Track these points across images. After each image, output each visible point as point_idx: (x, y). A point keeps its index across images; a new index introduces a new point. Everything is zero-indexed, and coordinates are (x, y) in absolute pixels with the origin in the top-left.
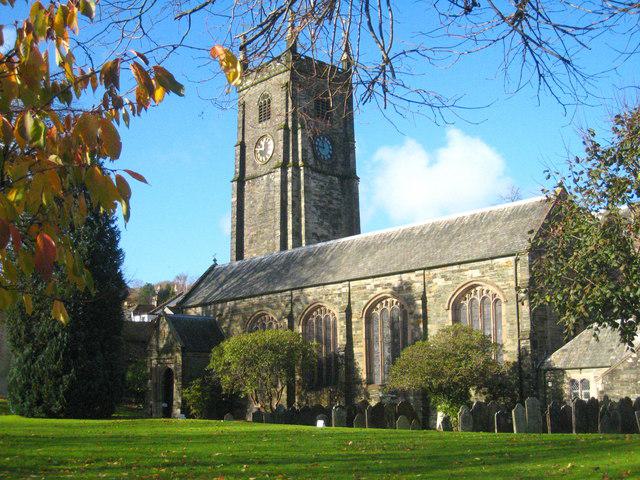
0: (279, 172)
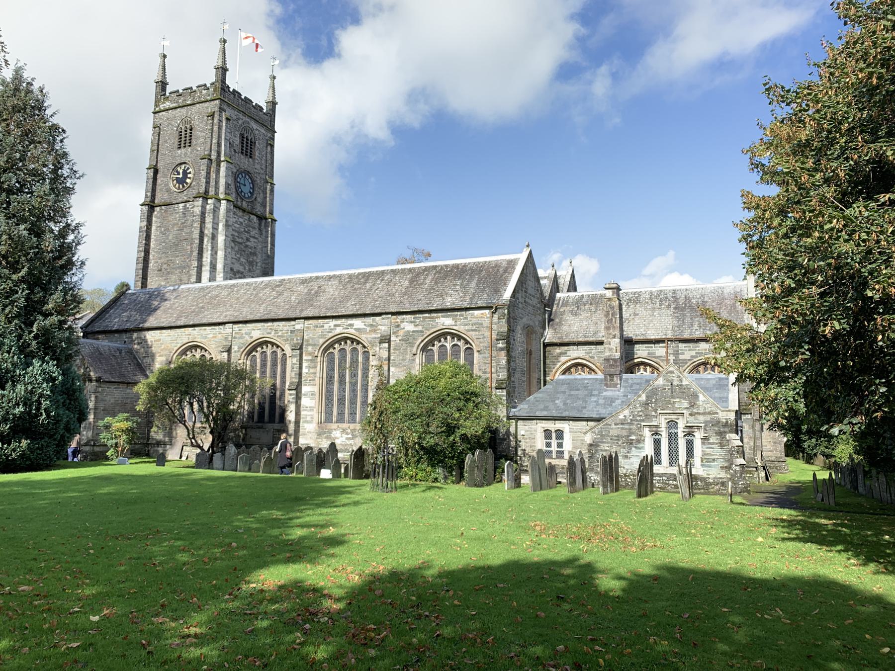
0: (199, 202)
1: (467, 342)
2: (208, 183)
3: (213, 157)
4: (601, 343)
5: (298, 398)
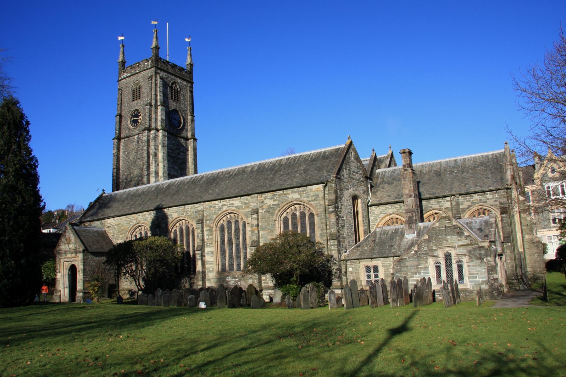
2: (150, 120)
3: (153, 104)
5: (203, 256)
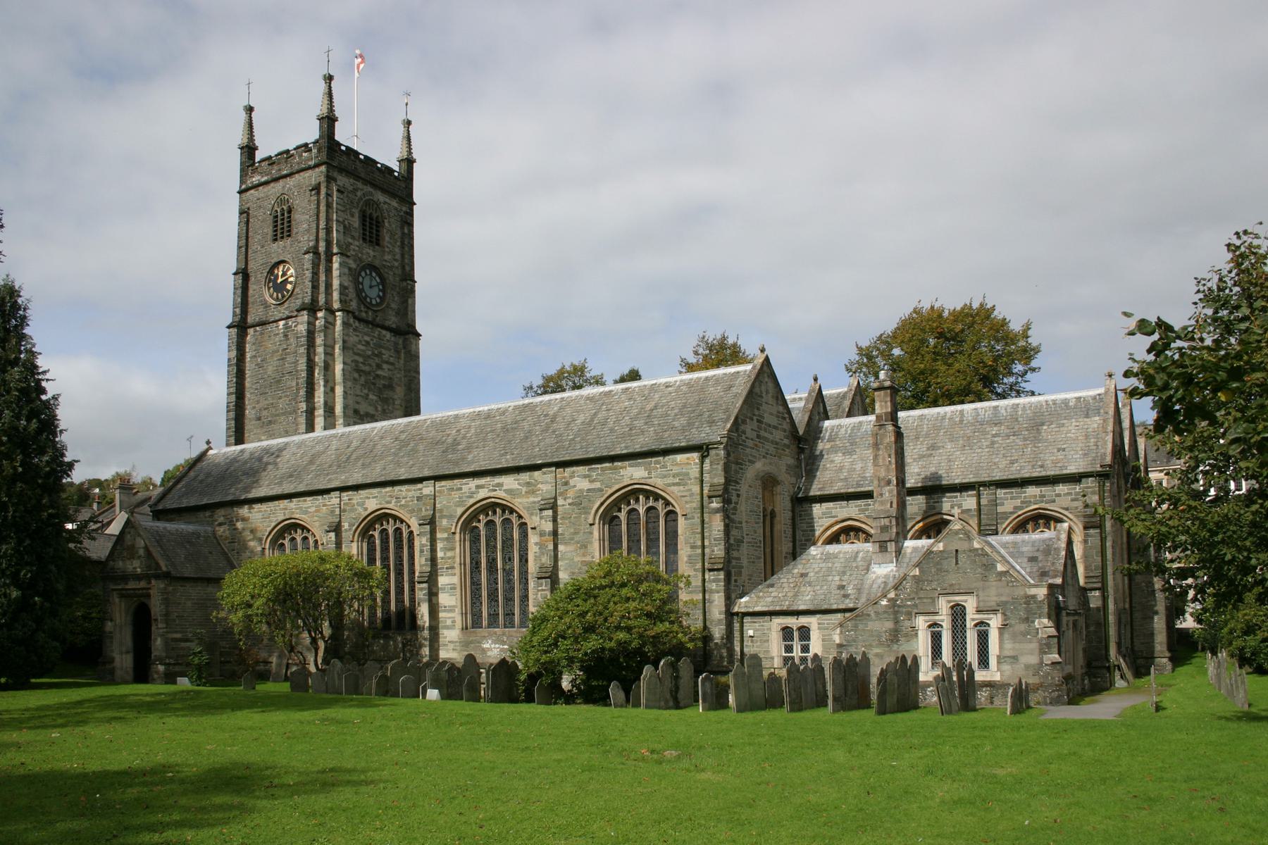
0: (304, 317)
1: (667, 503)
3: (322, 248)
4: (868, 495)
5: (433, 594)
